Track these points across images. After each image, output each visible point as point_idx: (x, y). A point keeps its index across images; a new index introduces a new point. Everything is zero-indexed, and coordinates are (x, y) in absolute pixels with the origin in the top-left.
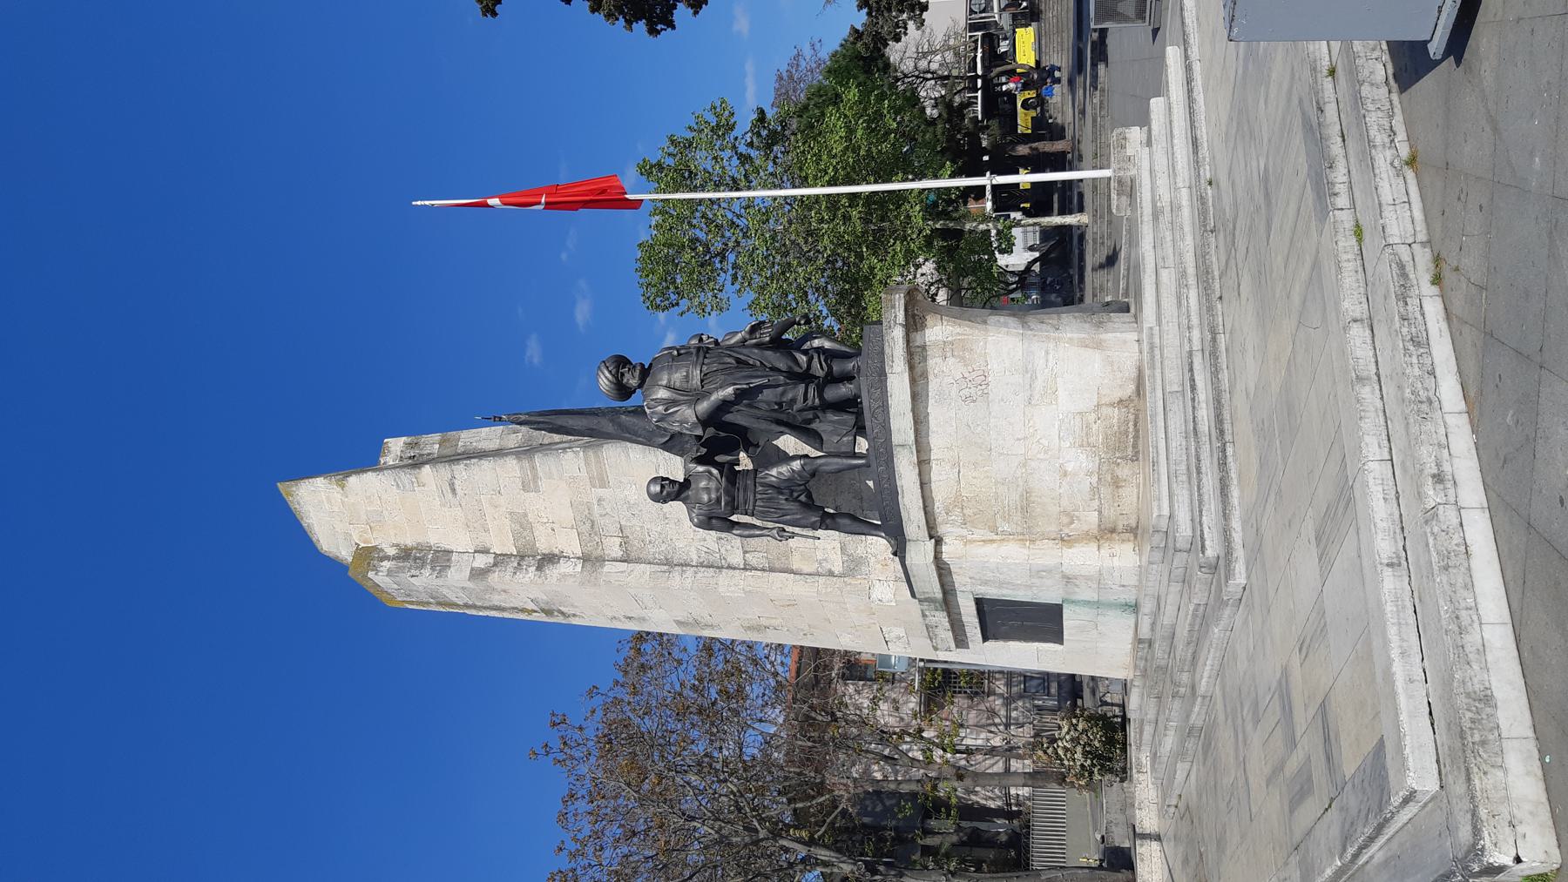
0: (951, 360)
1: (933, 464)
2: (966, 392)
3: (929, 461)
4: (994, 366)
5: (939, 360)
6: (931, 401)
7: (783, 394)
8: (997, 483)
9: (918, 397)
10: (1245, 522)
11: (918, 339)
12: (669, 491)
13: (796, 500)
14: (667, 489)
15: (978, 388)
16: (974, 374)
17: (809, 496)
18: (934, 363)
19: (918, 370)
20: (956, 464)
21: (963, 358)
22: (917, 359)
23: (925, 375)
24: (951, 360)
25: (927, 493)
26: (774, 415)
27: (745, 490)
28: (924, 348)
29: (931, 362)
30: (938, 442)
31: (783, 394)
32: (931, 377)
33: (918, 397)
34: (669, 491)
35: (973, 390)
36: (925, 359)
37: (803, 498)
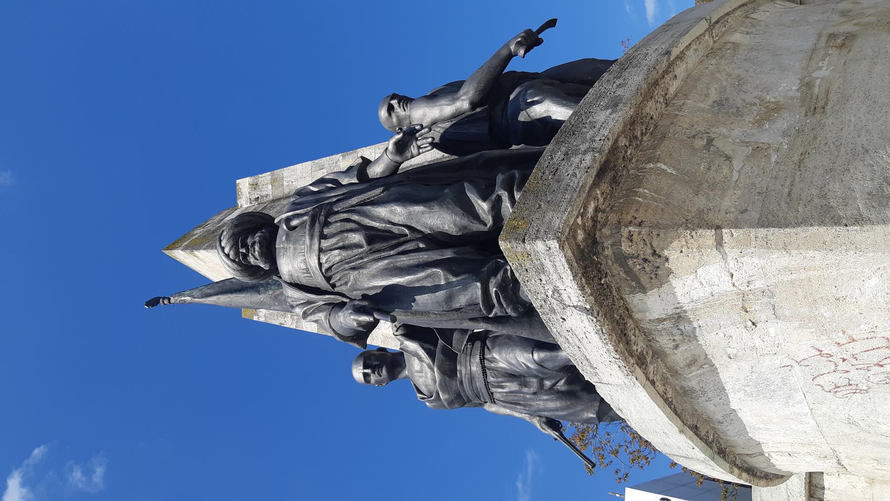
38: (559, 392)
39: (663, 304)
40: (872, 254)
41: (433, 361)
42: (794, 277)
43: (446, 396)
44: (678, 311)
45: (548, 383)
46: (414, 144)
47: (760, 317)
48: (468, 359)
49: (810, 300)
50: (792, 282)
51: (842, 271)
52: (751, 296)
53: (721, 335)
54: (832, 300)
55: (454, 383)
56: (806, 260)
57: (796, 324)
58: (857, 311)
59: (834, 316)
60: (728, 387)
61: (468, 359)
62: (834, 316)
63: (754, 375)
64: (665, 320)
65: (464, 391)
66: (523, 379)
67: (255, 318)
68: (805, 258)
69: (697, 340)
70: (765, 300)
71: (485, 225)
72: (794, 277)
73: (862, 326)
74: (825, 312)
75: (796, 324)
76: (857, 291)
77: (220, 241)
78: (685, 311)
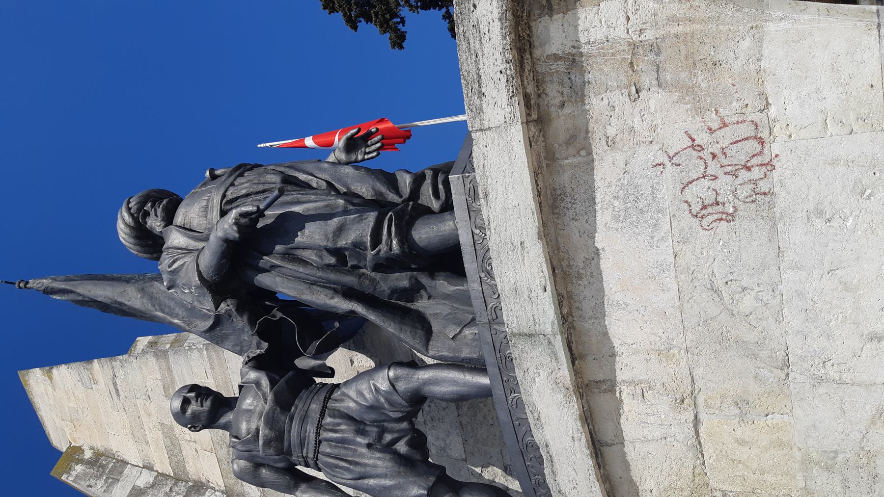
0: (654, 99)
1: (625, 393)
2: (700, 191)
3: (609, 385)
4: (788, 106)
5: (619, 98)
6: (603, 218)
7: (340, 230)
8: (807, 463)
9: (560, 204)
10: (159, 317)
11: (553, 34)
12: (206, 408)
13: (389, 449)
14: (193, 407)
15: (737, 177)
16: (726, 136)
17: (419, 442)
18: (608, 108)
19: (560, 124)
20: (687, 398)
21: (688, 91)
22: (553, 92)
23: (580, 140)
24: (654, 99)
25: (616, 471)
26: (332, 276)
27: (304, 420)
28: (574, 60)
29: (596, 104)
30: (635, 324)
31: (340, 230)
32: (598, 148)
33: (560, 204)
34: (206, 408)
35: (724, 184)
36: (577, 94)
37: (402, 447)
38: (396, 453)
39: (564, 36)
40: (746, 10)
41: (271, 389)
42: (680, 29)
43: (267, 432)
44: (574, 51)
45: (388, 437)
46: (363, 149)
47: (647, 80)
48: (311, 396)
49: (691, 61)
50: (677, 36)
51: (721, 27)
52: (641, 50)
53: (606, 101)
54: (710, 64)
55: (283, 418)
56: (692, 10)
57: (675, 96)
58: (730, 81)
59: (709, 87)
60: (599, 198)
61: (311, 396)
62: (709, 87)
63: (627, 177)
64: (561, 58)
65: (290, 432)
66: (362, 427)
67: (64, 478)
68: (691, 6)
69: (583, 101)
70: (652, 57)
71: (401, 196)
72: (680, 29)
73: (734, 104)
74: (702, 80)
75: (675, 96)
76: (732, 54)
77: (129, 202)
78: (581, 55)
